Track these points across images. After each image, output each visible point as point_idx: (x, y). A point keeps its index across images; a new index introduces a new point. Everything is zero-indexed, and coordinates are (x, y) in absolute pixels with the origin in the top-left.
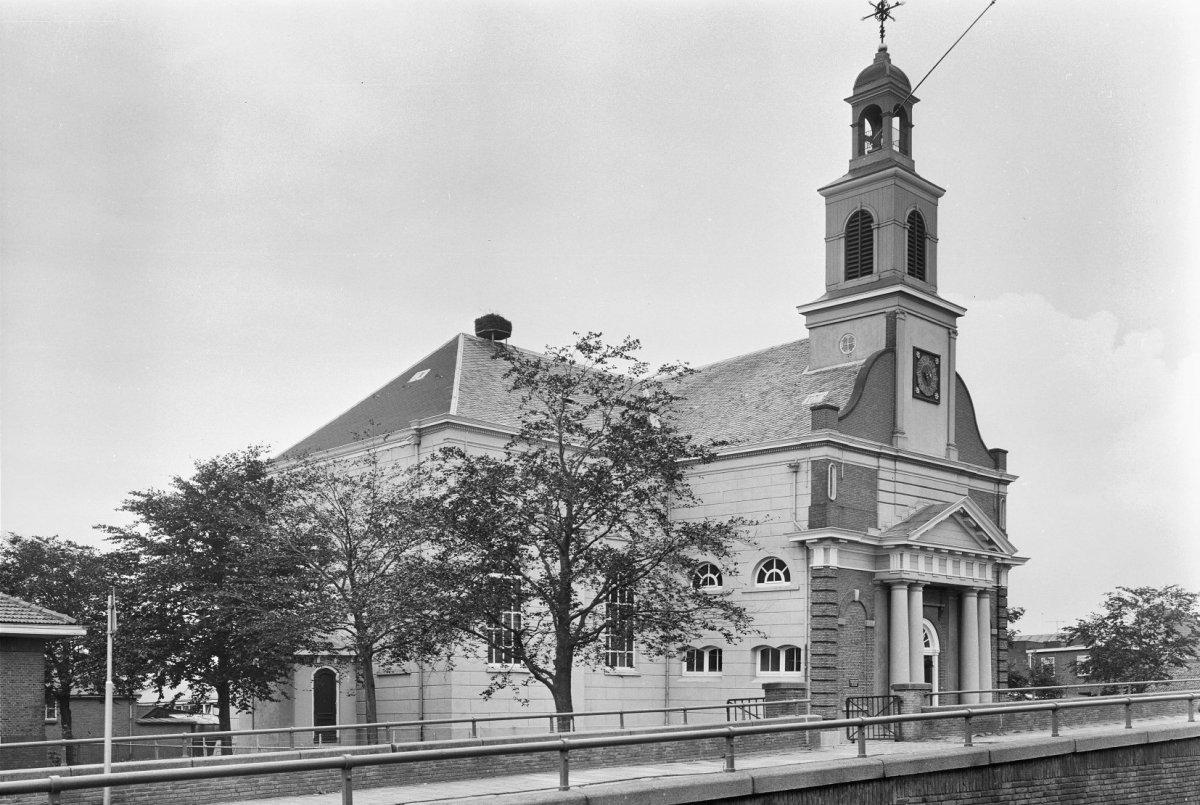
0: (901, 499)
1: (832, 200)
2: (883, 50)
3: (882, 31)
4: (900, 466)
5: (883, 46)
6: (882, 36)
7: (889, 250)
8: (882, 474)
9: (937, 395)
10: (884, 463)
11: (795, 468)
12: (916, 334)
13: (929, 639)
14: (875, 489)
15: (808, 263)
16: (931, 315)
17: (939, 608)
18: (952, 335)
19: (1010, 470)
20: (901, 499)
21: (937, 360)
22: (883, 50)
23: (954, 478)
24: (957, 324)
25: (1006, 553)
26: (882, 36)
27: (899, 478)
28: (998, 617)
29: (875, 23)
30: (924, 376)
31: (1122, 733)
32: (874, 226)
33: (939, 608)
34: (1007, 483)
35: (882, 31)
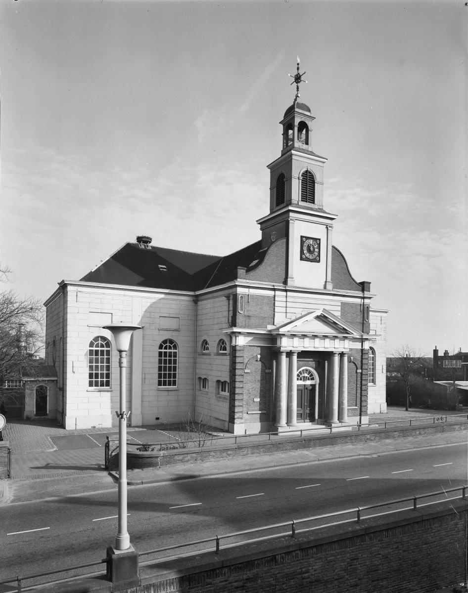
6: (298, 90)
11: (228, 297)
26: (298, 90)
30: (309, 251)
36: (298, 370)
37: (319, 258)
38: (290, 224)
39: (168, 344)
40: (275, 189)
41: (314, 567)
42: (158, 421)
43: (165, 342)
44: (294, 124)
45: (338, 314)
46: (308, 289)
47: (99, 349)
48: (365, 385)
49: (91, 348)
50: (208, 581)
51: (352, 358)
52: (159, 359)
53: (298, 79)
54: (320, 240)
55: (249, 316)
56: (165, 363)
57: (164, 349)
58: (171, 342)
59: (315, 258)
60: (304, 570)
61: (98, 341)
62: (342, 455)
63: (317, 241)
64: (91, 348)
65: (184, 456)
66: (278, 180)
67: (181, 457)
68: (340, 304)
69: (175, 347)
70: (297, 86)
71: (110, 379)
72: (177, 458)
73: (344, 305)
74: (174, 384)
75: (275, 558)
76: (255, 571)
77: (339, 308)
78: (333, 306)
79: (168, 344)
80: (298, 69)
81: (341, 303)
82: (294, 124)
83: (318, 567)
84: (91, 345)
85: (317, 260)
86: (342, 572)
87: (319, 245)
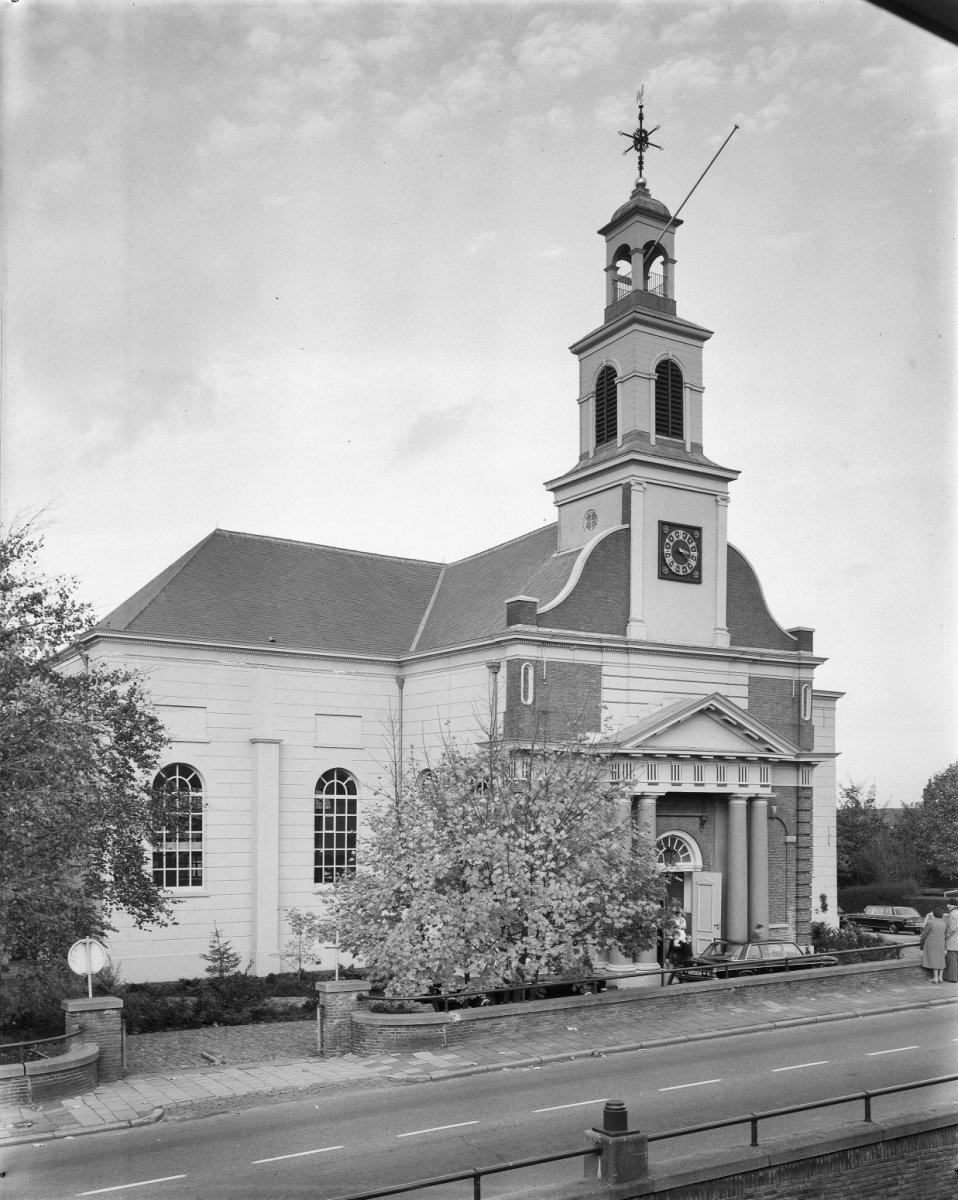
0: (634, 697)
1: (583, 355)
2: (641, 186)
3: (641, 163)
4: (634, 659)
5: (641, 181)
6: (641, 168)
7: (636, 408)
8: (605, 670)
9: (697, 574)
10: (608, 657)
11: (494, 668)
12: (652, 506)
13: (690, 852)
14: (596, 689)
15: (560, 436)
16: (588, 489)
17: (701, 817)
18: (722, 503)
19: (817, 652)
20: (634, 697)
21: (697, 533)
22: (641, 186)
23: (724, 666)
24: (729, 490)
25: (786, 752)
26: (641, 168)
27: (634, 672)
28: (798, 810)
29: (635, 154)
30: (676, 554)
31: (861, 1131)
32: (616, 380)
33: (701, 817)
34: (813, 666)
35: (641, 163)
36: (657, 836)
37: (700, 572)
38: (633, 493)
39: (177, 777)
40: (592, 403)
41: (905, 1176)
42: (318, 966)
43: (328, 775)
44: (641, 231)
45: (744, 704)
46: (695, 648)
47: (335, 797)
48: (804, 873)
49: (352, 797)
50: (748, 1191)
51: (775, 808)
52: (316, 817)
53: (641, 140)
54: (699, 529)
55: (545, 713)
56: (340, 821)
57: (327, 793)
58: (343, 774)
59: (691, 574)
60: (889, 1179)
61: (175, 774)
62: (792, 1016)
63: (694, 531)
64: (352, 797)
65: (495, 1021)
66: (599, 379)
67: (487, 1025)
68: (746, 682)
69: (352, 789)
70: (641, 158)
71: (685, 844)
72: (479, 1025)
73: (754, 683)
74: (198, 881)
75: (846, 1157)
76: (814, 1178)
77: (745, 691)
78: (732, 684)
79: (177, 777)
80: (641, 118)
81: (750, 678)
82: (641, 231)
83: (911, 1175)
84: (319, 787)
85: (694, 578)
86: (948, 1187)
87: (699, 541)
